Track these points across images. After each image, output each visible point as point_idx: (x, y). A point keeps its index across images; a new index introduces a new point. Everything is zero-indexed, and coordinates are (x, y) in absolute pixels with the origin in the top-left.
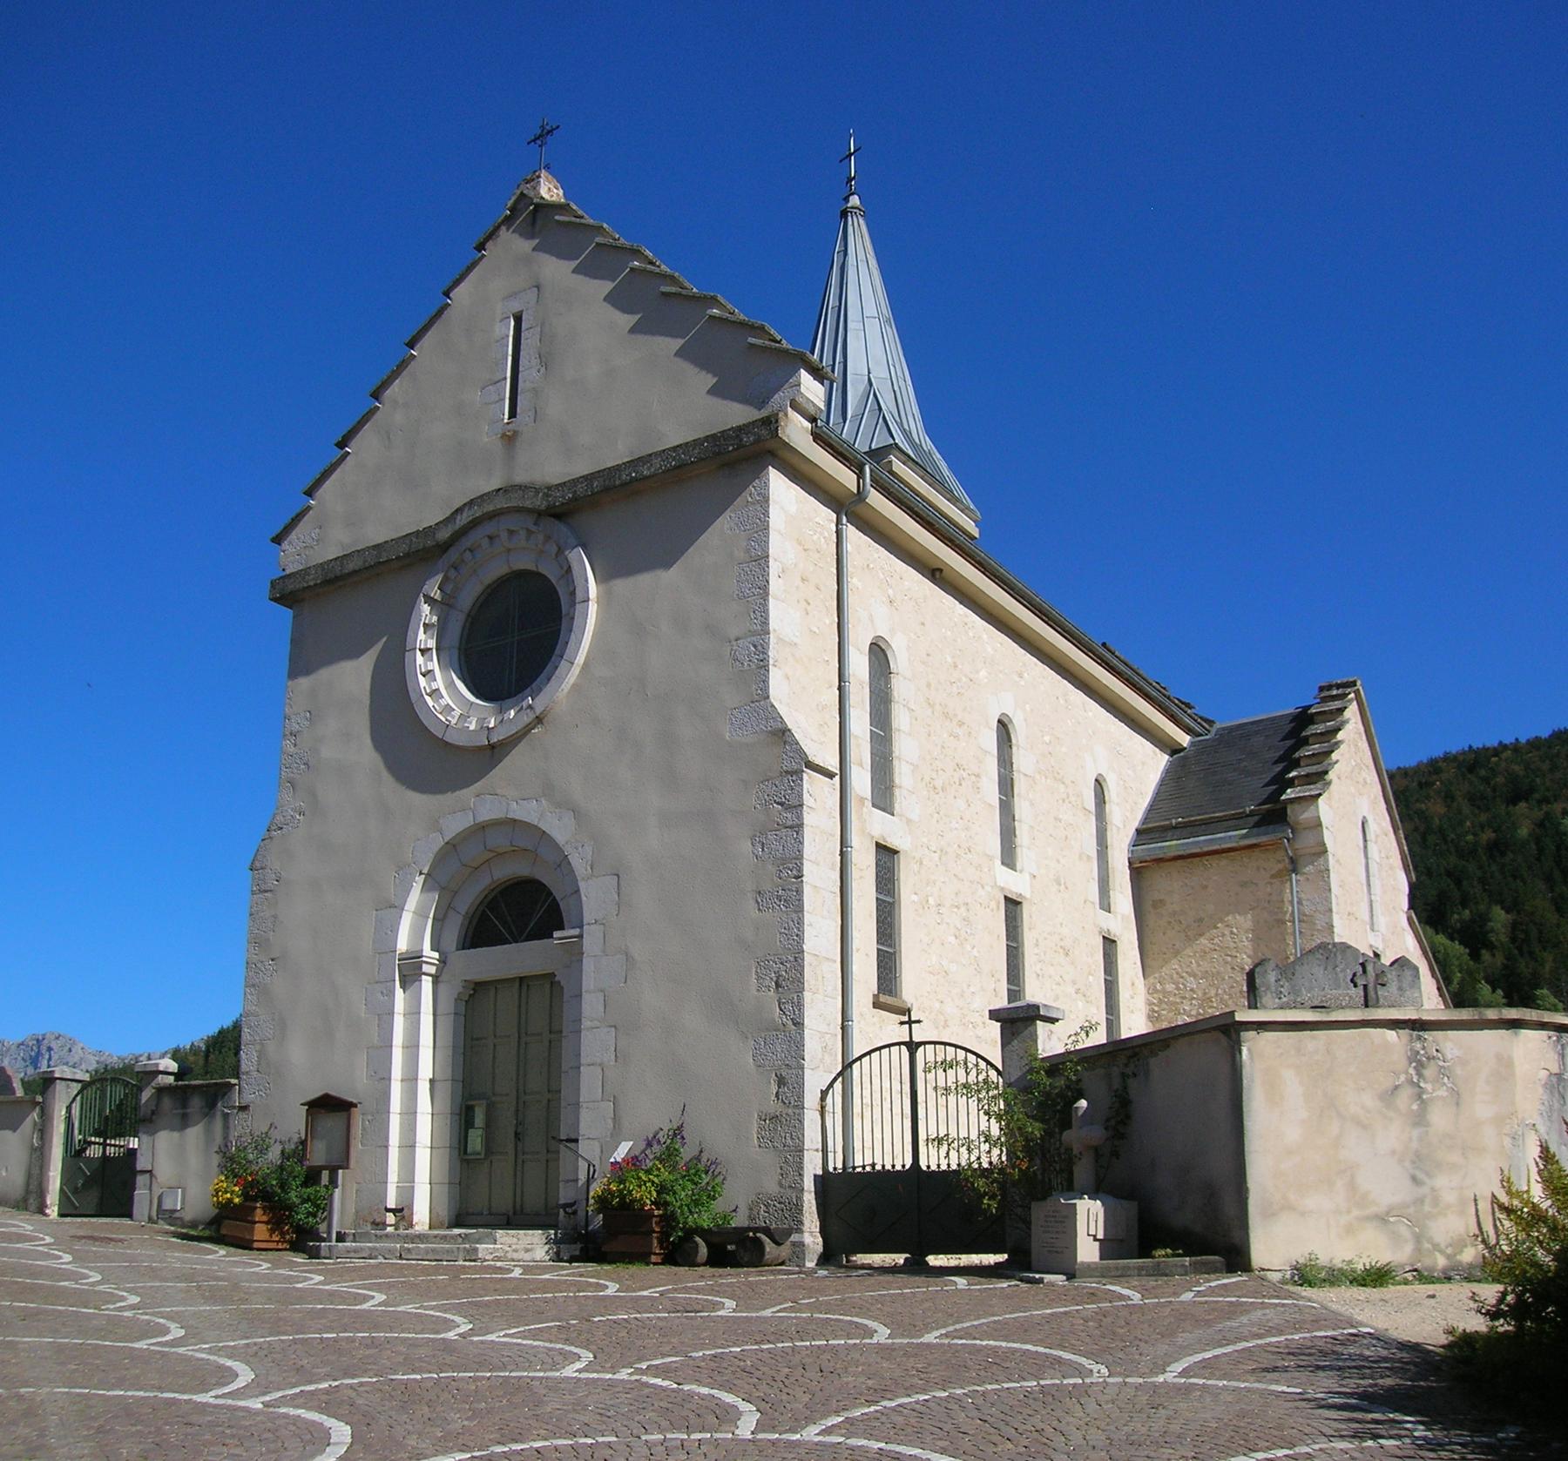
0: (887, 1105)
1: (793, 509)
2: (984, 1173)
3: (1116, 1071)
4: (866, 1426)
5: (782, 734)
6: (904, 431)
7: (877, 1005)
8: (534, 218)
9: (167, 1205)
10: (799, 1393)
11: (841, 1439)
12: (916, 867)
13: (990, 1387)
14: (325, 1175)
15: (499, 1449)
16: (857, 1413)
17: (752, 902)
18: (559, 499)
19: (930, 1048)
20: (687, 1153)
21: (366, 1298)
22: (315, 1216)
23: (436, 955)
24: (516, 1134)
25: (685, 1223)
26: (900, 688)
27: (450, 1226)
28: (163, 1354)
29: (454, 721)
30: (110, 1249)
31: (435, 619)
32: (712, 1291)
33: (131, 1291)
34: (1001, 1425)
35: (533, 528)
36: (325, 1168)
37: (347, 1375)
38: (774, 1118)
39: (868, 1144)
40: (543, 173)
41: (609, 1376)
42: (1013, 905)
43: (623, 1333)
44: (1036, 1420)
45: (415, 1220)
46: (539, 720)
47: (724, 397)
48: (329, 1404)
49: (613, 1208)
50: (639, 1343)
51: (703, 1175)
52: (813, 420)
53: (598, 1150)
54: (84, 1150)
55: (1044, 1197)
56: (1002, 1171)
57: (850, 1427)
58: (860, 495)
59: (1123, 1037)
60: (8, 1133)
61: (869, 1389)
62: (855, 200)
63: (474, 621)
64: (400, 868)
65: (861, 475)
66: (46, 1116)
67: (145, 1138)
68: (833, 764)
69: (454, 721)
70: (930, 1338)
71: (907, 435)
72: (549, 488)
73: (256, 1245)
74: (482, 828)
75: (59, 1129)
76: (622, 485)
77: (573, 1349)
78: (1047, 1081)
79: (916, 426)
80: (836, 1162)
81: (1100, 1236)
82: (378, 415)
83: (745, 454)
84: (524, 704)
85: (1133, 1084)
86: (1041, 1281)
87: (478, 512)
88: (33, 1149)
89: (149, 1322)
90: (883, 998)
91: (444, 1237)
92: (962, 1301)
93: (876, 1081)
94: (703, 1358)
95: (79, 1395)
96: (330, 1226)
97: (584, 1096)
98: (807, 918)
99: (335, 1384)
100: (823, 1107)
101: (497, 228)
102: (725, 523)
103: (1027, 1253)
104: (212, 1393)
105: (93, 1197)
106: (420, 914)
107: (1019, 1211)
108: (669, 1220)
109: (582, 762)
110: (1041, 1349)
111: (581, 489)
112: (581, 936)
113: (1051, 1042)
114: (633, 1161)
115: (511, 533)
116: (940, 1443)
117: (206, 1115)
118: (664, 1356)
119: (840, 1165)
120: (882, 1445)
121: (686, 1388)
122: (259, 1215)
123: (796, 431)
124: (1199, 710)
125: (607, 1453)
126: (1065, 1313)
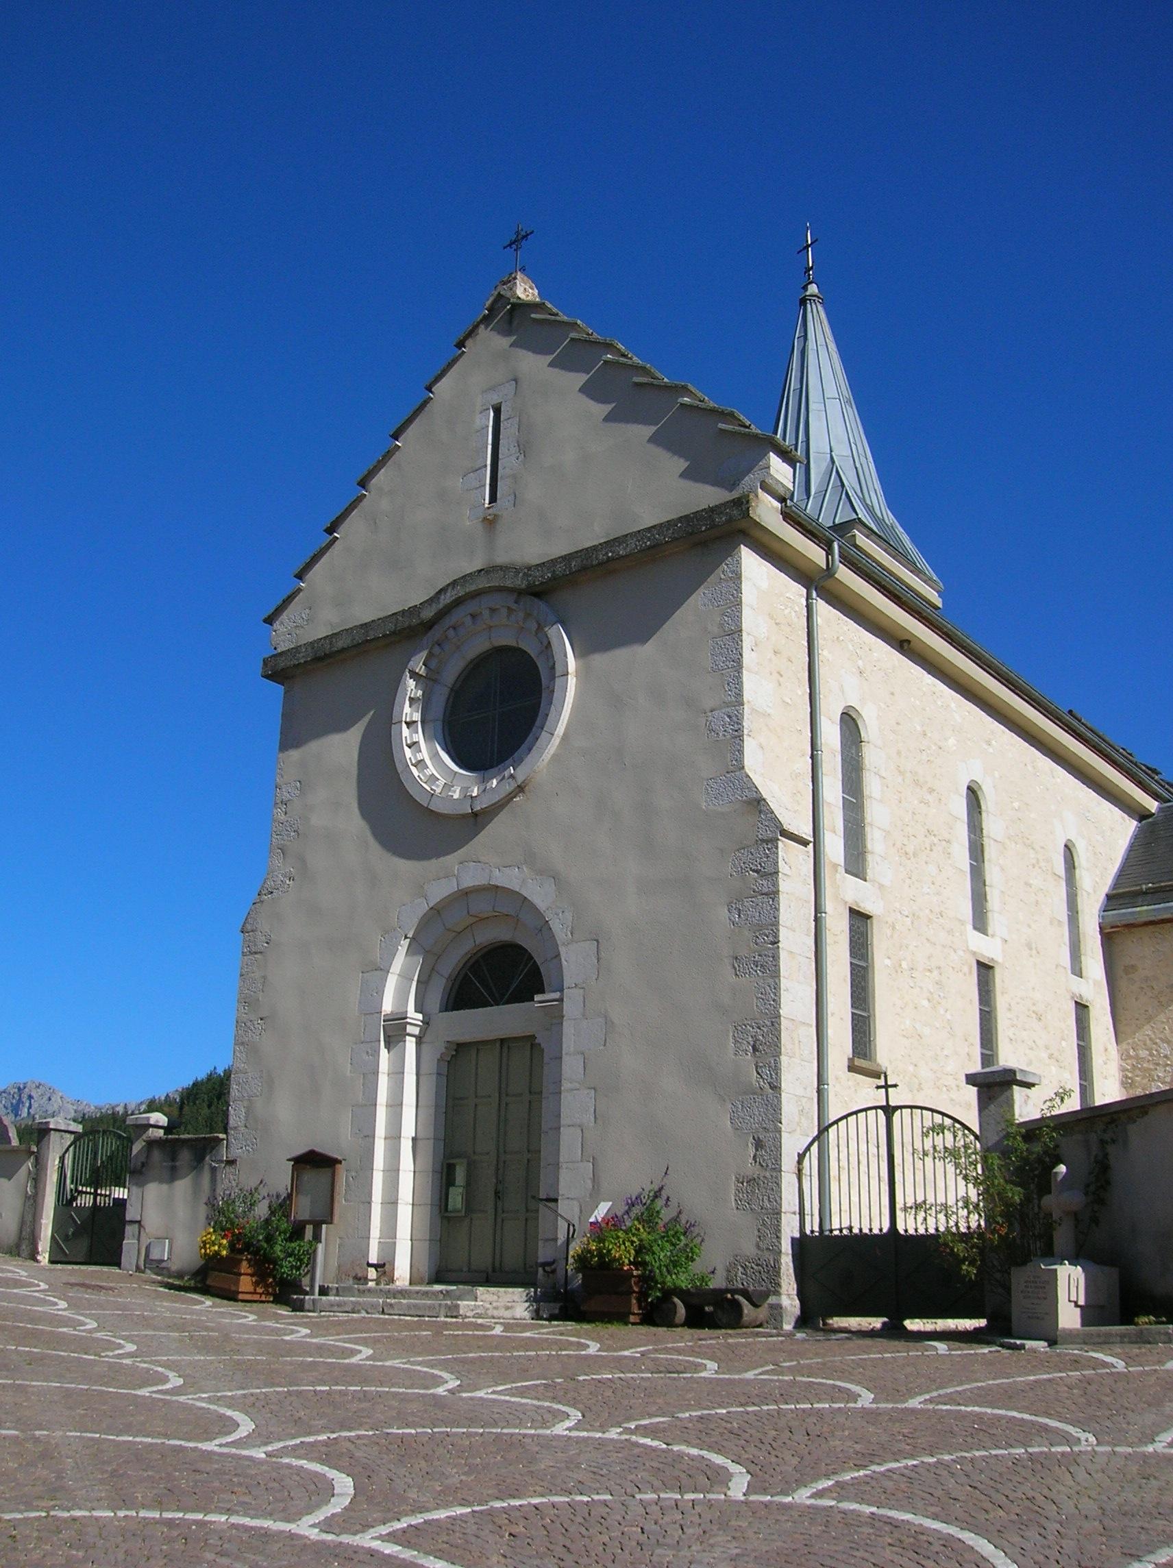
0: (863, 1168)
1: (764, 585)
2: (965, 1237)
3: (1094, 1138)
4: (857, 1490)
5: (757, 804)
6: (866, 506)
7: (852, 1068)
8: (511, 317)
9: (155, 1255)
10: (787, 1455)
11: (833, 1503)
12: (889, 932)
13: (977, 1454)
14: (309, 1230)
15: (498, 1504)
16: (847, 1477)
17: (730, 968)
18: (538, 578)
19: (906, 1112)
20: (666, 1215)
21: (354, 1352)
22: (298, 1269)
23: (420, 1016)
24: (497, 1193)
25: (664, 1283)
26: (872, 756)
27: (430, 1283)
28: (165, 1402)
29: (438, 790)
30: (102, 1297)
31: (420, 693)
32: (692, 1352)
33: (128, 1339)
34: (993, 1493)
35: (514, 606)
36: (309, 1222)
37: (343, 1427)
38: (751, 1181)
39: (845, 1207)
40: (519, 275)
41: (599, 1435)
42: (985, 969)
43: (609, 1393)
44: (1026, 1488)
45: (396, 1275)
46: (521, 789)
47: (696, 480)
48: (329, 1454)
49: (592, 1268)
50: (625, 1402)
51: (683, 1237)
52: (782, 500)
53: (577, 1210)
54: (75, 1199)
55: (1024, 1262)
56: (981, 1235)
57: (841, 1491)
58: (829, 571)
59: (1097, 1104)
60: (3, 1181)
61: (857, 1453)
62: (813, 289)
63: (457, 693)
64: (386, 932)
65: (829, 552)
66: (40, 1164)
67: (134, 1189)
68: (806, 831)
69: (438, 790)
70: (914, 1403)
71: (870, 509)
72: (529, 568)
73: (241, 1297)
74: (465, 894)
75: (52, 1178)
76: (599, 564)
77: (560, 1407)
78: (1023, 1146)
79: (877, 499)
80: (813, 1225)
81: (1082, 1302)
82: (365, 502)
83: (715, 536)
84: (506, 774)
85: (1111, 1149)
86: (1022, 1347)
87: (460, 591)
88: (27, 1197)
89: (148, 1370)
90: (858, 1062)
91: (426, 1293)
92: (942, 1366)
93: (853, 1145)
94: (690, 1419)
95: (92, 1439)
96: (313, 1280)
97: (564, 1156)
98: (784, 983)
99: (333, 1436)
100: (800, 1170)
101: (476, 327)
102: (699, 599)
103: (1008, 1319)
104: (217, 1442)
105: (83, 1245)
106: (405, 977)
107: (998, 1276)
108: (648, 1280)
109: (564, 828)
110: (1026, 1417)
111: (559, 569)
112: (561, 1000)
113: (1027, 1107)
114: (613, 1221)
115: (493, 610)
116: (933, 1509)
117: (195, 1168)
118: (651, 1416)
119: (816, 1228)
120: (874, 1509)
121: (675, 1448)
122: (244, 1267)
123: (767, 511)
124: (1164, 776)
125: (604, 1511)
126: (1049, 1380)
